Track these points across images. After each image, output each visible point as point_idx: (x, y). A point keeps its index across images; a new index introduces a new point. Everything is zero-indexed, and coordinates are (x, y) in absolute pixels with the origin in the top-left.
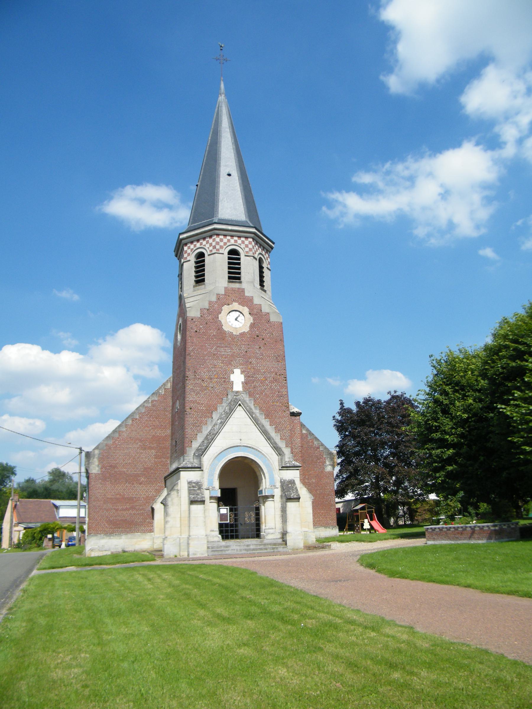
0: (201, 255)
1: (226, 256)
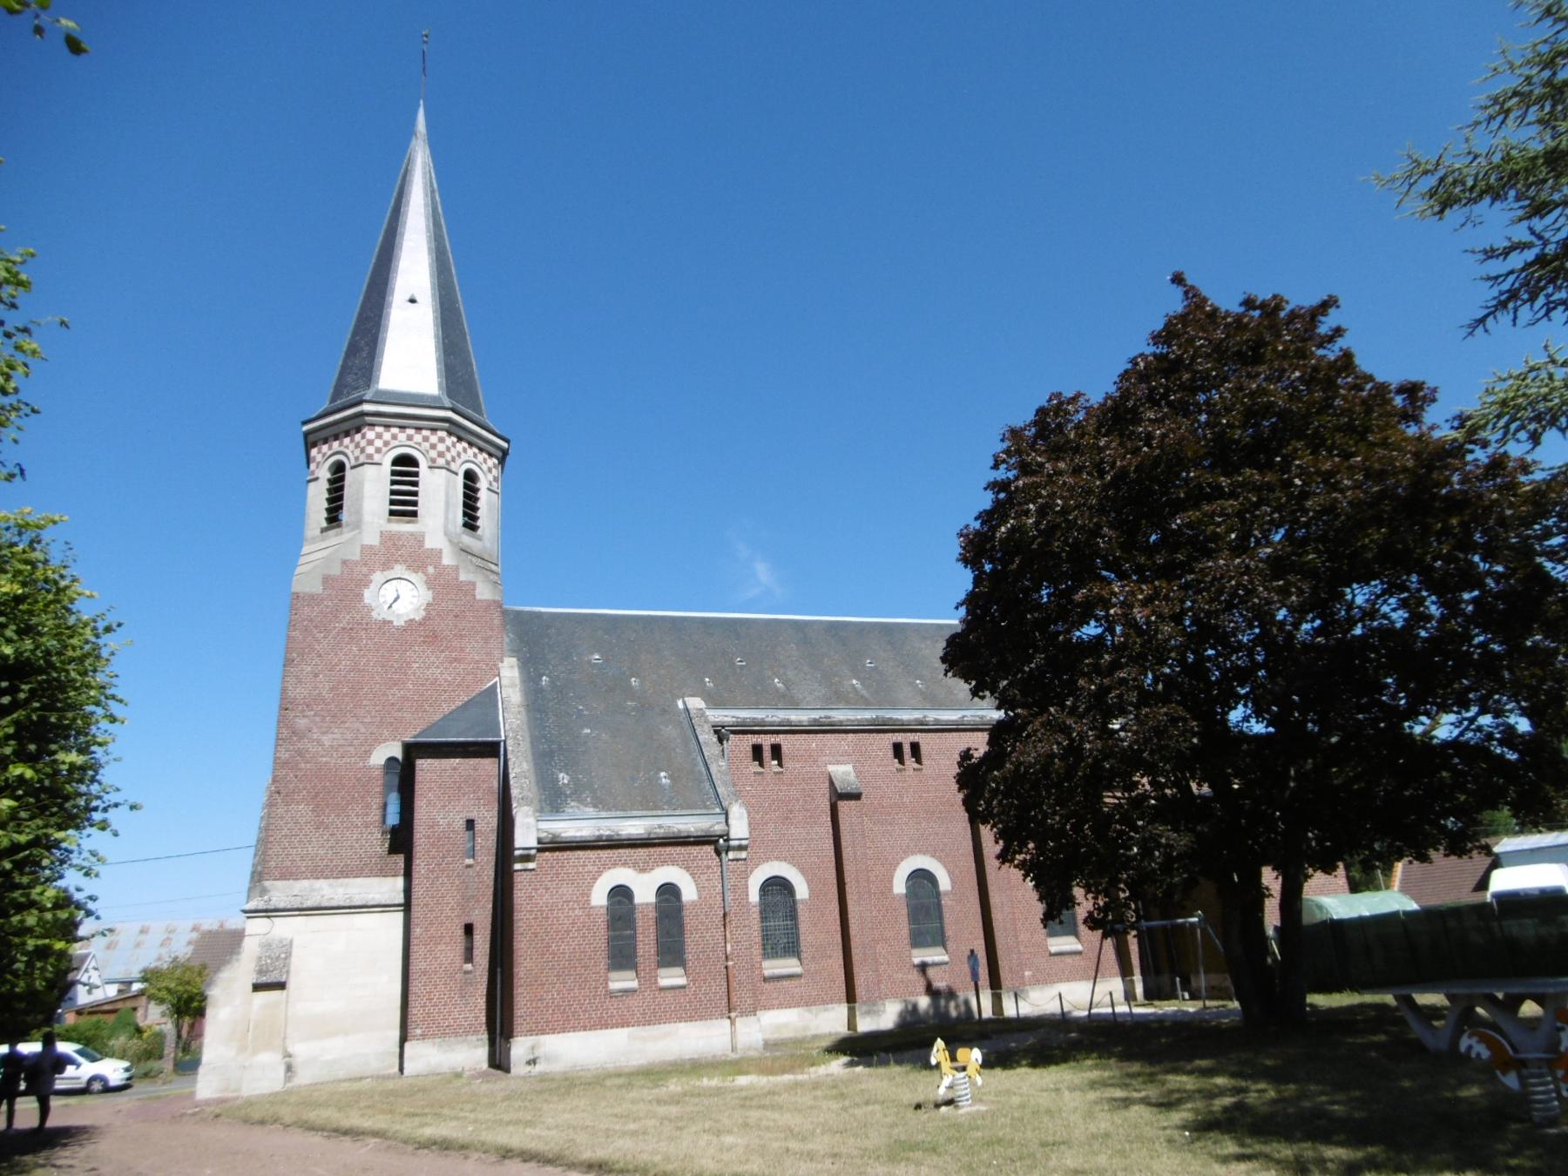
0: (339, 468)
1: (387, 467)
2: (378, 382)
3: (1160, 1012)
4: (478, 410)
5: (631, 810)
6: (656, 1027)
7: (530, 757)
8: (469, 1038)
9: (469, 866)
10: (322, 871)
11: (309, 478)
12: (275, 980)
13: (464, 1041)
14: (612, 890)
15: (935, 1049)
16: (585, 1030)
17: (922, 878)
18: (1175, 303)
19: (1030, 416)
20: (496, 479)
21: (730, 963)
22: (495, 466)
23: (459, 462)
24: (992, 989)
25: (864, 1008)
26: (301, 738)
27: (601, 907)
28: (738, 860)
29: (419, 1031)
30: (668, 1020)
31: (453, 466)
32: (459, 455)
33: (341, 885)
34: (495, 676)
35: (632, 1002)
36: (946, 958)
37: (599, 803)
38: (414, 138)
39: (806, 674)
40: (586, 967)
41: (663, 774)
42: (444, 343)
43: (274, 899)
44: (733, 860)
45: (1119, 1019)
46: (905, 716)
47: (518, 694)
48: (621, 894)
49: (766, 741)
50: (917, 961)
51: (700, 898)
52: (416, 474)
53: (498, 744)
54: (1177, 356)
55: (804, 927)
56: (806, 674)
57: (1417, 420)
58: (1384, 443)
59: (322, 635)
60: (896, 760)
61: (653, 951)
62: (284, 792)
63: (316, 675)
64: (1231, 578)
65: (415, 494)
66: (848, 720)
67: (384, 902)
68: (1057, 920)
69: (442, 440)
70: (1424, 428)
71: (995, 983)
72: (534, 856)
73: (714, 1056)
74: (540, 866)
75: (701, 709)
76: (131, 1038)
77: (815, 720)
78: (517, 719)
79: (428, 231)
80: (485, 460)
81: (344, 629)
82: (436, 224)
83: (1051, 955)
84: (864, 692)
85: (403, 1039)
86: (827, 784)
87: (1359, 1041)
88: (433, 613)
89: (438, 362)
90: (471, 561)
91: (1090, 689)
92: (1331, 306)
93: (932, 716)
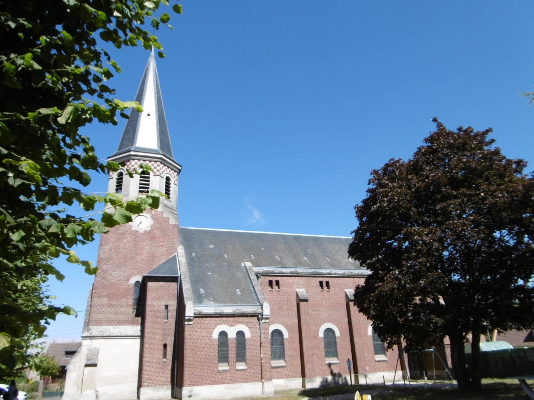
2: (136, 144)
3: (418, 384)
4: (171, 155)
5: (227, 303)
6: (235, 384)
7: (190, 283)
8: (164, 386)
9: (166, 322)
10: (111, 323)
11: (109, 178)
12: (93, 363)
13: (162, 388)
14: (220, 333)
15: (356, 395)
16: (209, 385)
17: (329, 331)
18: (433, 129)
19: (382, 165)
20: (176, 180)
21: (262, 361)
22: (176, 175)
23: (164, 173)
24: (354, 373)
25: (309, 379)
26: (105, 273)
27: (216, 339)
28: (266, 323)
29: (146, 384)
30: (240, 382)
31: (162, 175)
32: (164, 171)
33: (117, 328)
34: (175, 252)
35: (227, 375)
36: (338, 362)
37: (215, 300)
38: (150, 57)
39: (287, 255)
40: (210, 361)
41: (238, 290)
42: (160, 130)
43: (93, 332)
44: (264, 323)
45: (407, 386)
46: (324, 271)
47: (185, 259)
48: (223, 334)
49: (274, 279)
50: (327, 362)
51: (252, 336)
52: (149, 178)
53: (177, 277)
54: (436, 147)
55: (286, 348)
56: (287, 255)
57: (520, 172)
58: (510, 181)
59: (113, 235)
60: (320, 288)
61: (234, 356)
62: (98, 293)
63: (111, 250)
64: (459, 227)
65: (148, 185)
66: (304, 272)
67: (133, 335)
68: (391, 349)
69: (158, 166)
70: (523, 175)
71: (356, 371)
72: (193, 319)
73: (256, 396)
74: (194, 323)
75: (251, 267)
76: (26, 383)
77: (292, 272)
78: (185, 268)
79: (155, 90)
80: (173, 173)
81: (121, 233)
82: (157, 88)
83: (376, 361)
84: (308, 262)
85: (139, 386)
86: (295, 296)
87: (504, 396)
88: (154, 228)
89: (158, 137)
90: (168, 210)
91: (408, 265)
92: (490, 131)
93: (334, 271)
